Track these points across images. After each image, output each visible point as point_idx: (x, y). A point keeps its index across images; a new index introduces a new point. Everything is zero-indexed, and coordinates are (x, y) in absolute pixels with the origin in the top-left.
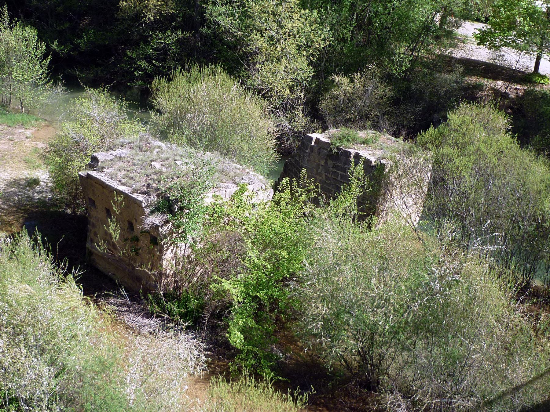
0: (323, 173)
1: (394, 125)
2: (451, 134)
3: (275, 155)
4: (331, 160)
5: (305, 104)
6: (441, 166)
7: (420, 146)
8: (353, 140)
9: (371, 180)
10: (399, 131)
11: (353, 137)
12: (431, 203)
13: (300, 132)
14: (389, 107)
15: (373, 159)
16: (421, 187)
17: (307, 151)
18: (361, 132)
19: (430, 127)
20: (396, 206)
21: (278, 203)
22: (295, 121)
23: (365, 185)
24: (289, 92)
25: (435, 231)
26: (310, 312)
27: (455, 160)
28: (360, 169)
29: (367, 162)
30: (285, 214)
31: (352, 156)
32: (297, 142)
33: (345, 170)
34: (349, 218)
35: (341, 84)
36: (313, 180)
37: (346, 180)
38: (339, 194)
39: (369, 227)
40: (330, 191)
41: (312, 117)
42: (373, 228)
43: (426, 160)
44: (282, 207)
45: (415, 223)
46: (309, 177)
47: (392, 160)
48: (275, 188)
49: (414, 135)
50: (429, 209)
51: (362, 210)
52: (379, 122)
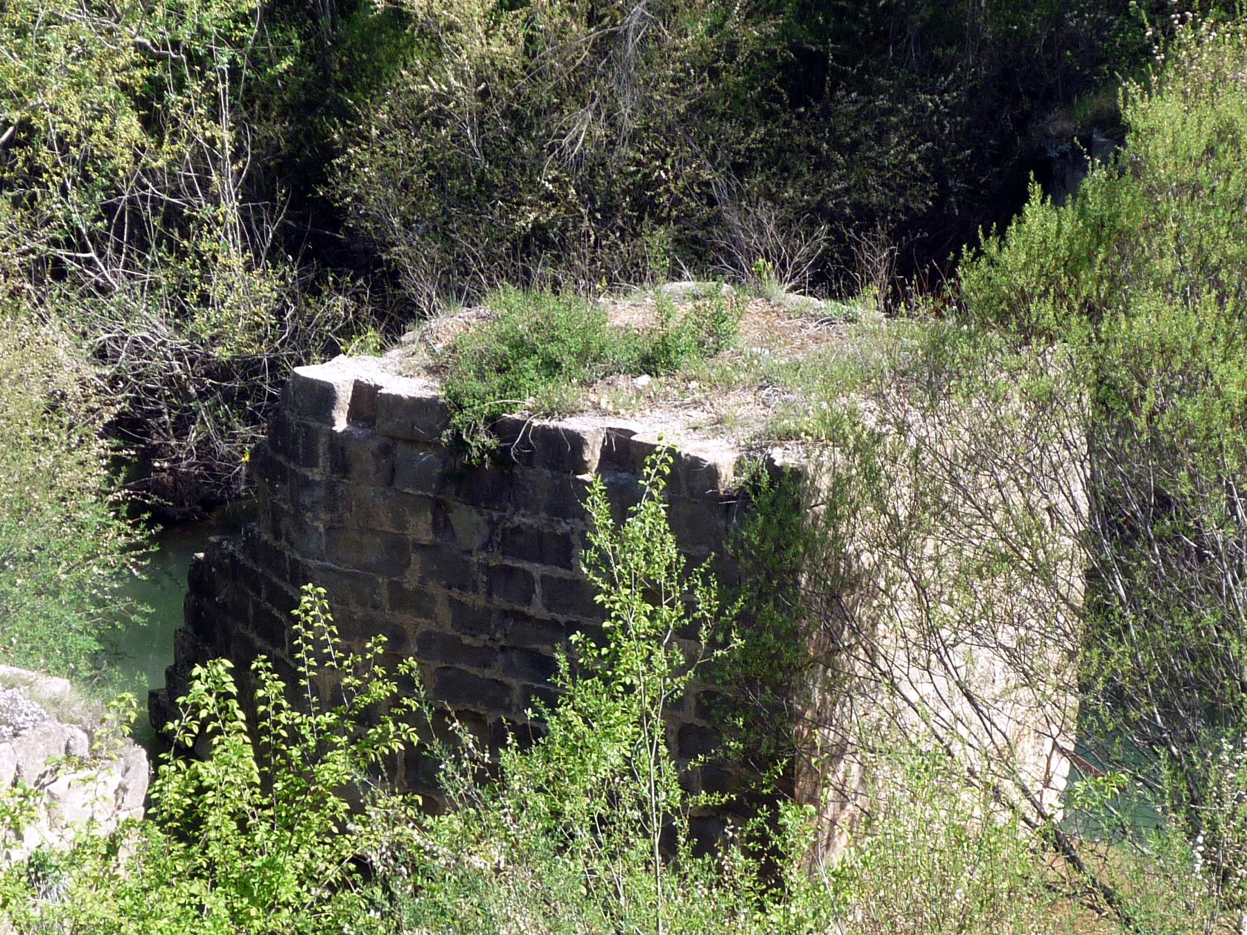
0: (437, 590)
1: (812, 223)
2: (1162, 220)
3: (117, 534)
4: (473, 501)
5: (255, 190)
6: (1141, 423)
7: (984, 325)
8: (582, 356)
9: (729, 586)
10: (847, 252)
11: (575, 344)
12: (1122, 658)
13: (250, 367)
14: (768, 116)
15: (721, 455)
16: (1043, 572)
17: (316, 474)
18: (624, 303)
19: (1025, 198)
20: (910, 716)
21: (187, 828)
22: (204, 300)
23: (696, 624)
24: (136, 131)
25: (1175, 823)
26: (53, 81)
27: (1220, 370)
28: (650, 528)
29: (689, 478)
30: (243, 887)
31: (592, 456)
32: (242, 430)
33: (563, 551)
34: (642, 845)
35: (451, 27)
36: (376, 645)
37: (580, 610)
38: (552, 704)
39: (770, 874)
40: (497, 695)
41: (306, 260)
42: (794, 875)
43: (1045, 402)
44: (214, 851)
45: (1050, 799)
46: (353, 632)
47: (836, 438)
48: (155, 739)
49: (942, 260)
50: (1118, 697)
51: (713, 779)
52: (718, 220)
